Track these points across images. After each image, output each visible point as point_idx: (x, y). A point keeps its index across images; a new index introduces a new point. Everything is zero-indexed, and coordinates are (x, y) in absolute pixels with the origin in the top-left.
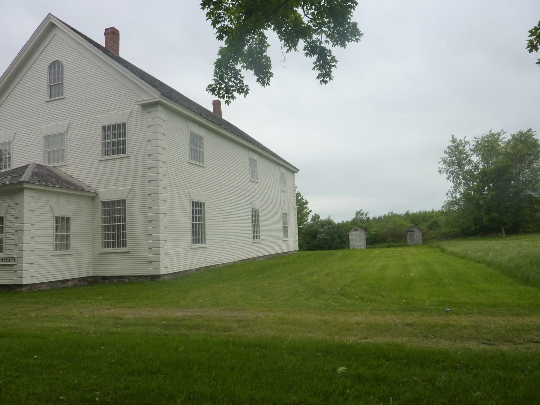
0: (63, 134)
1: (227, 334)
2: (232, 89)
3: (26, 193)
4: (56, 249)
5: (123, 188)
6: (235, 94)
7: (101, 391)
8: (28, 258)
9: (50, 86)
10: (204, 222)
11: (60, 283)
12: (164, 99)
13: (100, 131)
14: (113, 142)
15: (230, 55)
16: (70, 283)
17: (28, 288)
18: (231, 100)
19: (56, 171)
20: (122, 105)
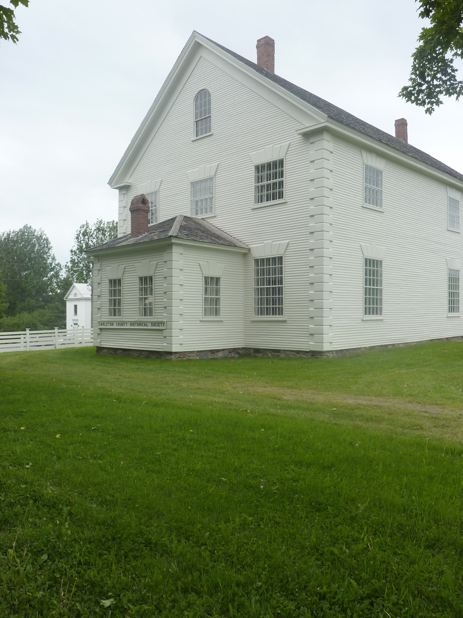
0: (211, 179)
1: (418, 433)
2: (437, 89)
3: (175, 250)
4: (205, 315)
5: (278, 242)
6: (442, 97)
7: (266, 479)
8: (177, 323)
9: (197, 122)
10: (381, 286)
11: (209, 353)
12: (332, 123)
13: (252, 173)
14: (268, 185)
15: (439, 38)
16: (220, 354)
17: (177, 356)
18: (435, 106)
19: (204, 223)
20: (277, 137)
